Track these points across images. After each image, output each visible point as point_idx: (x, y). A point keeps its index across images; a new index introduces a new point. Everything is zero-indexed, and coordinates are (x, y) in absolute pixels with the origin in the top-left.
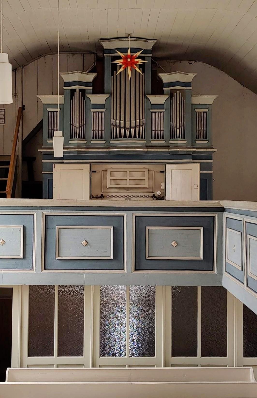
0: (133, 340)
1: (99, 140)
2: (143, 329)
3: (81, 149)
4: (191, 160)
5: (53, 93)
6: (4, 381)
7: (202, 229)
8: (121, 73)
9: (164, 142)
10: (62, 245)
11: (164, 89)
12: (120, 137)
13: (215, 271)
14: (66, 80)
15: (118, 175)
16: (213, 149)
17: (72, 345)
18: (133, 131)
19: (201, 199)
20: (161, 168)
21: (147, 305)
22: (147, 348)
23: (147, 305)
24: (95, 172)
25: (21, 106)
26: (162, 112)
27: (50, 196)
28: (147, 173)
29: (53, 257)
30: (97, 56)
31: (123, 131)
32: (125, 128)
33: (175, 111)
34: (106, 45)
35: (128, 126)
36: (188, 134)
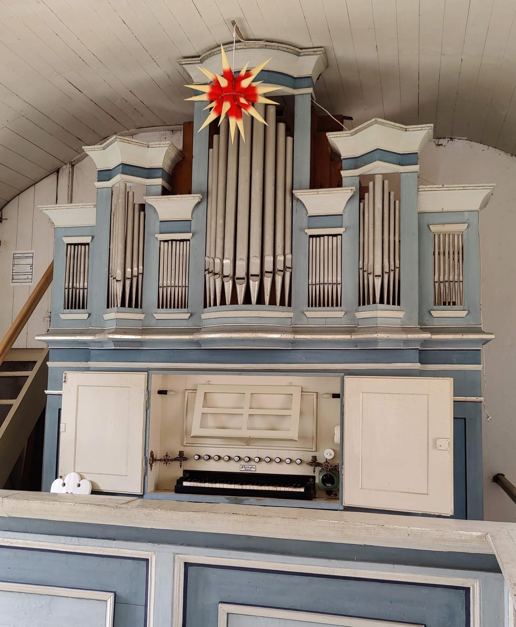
1: (176, 310)
3: (125, 333)
4: (417, 366)
9: (341, 314)
16: (483, 333)
18: (254, 286)
26: (336, 235)
33: (371, 230)
35: (241, 272)
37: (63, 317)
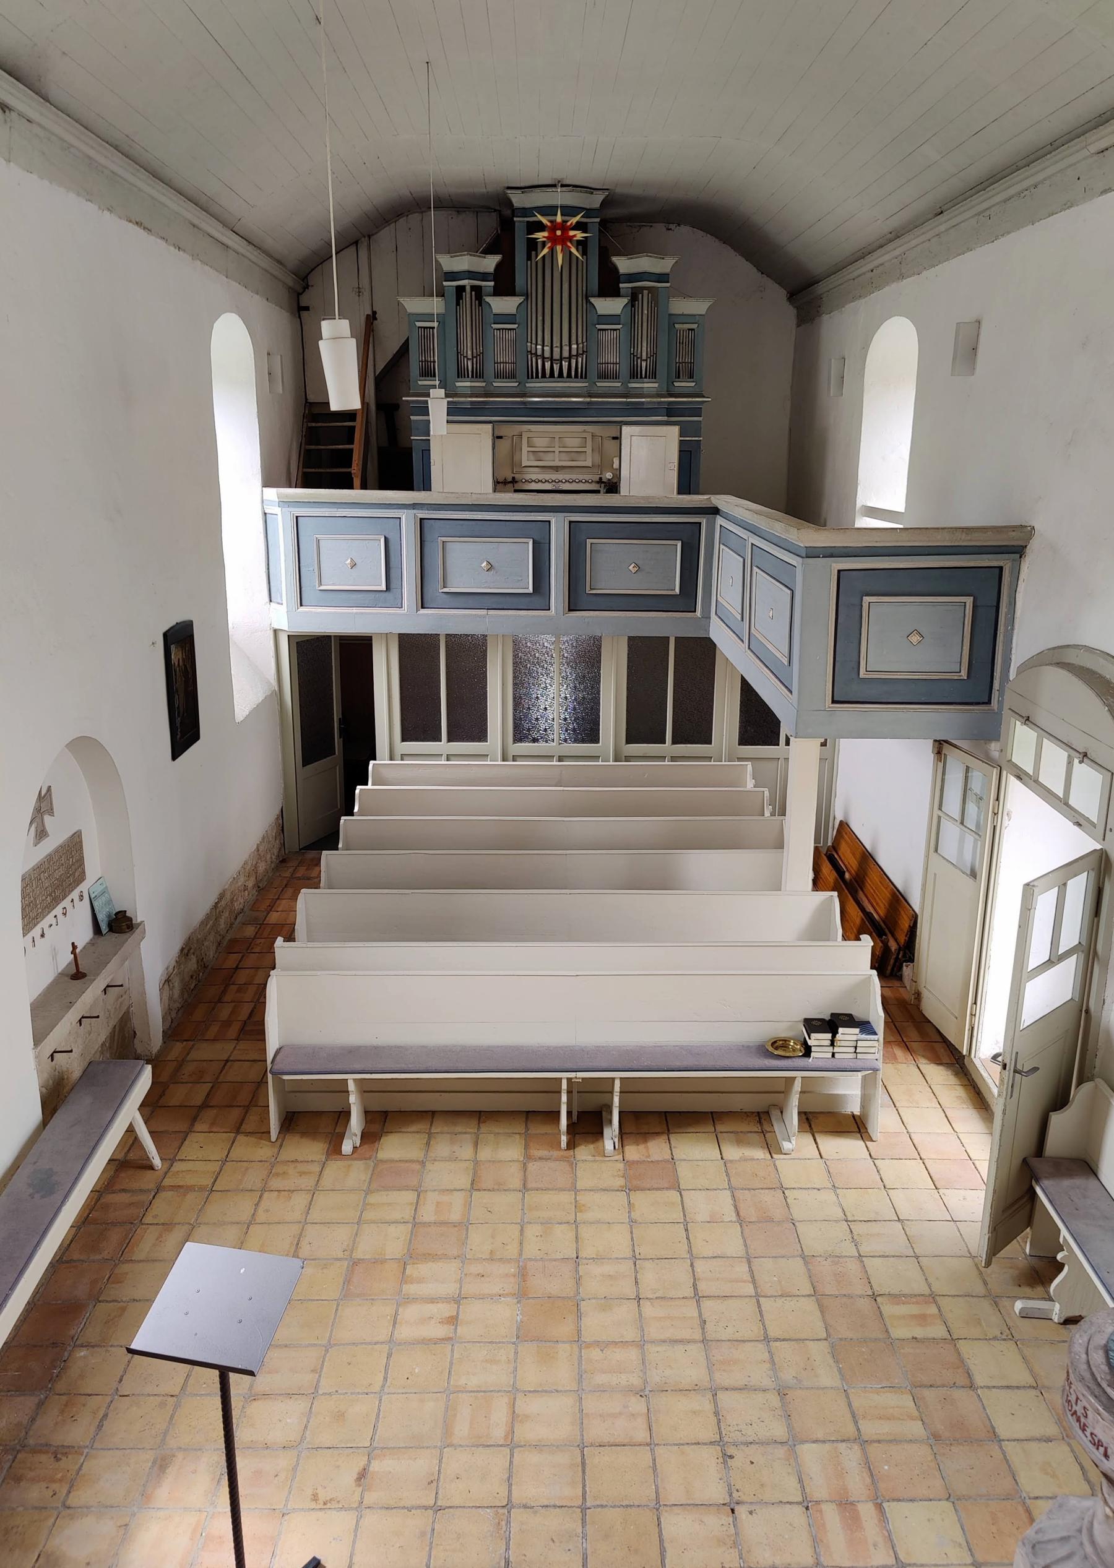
0: (565, 719)
2: (580, 702)
4: (665, 418)
5: (427, 293)
6: (367, 784)
8: (544, 257)
11: (621, 285)
12: (544, 376)
13: (698, 613)
14: (446, 268)
15: (541, 443)
17: (470, 725)
18: (565, 364)
19: (679, 493)
20: (612, 431)
21: (588, 661)
22: (586, 728)
23: (588, 661)
24: (501, 437)
25: (370, 313)
27: (427, 486)
29: (436, 589)
30: (500, 215)
31: (548, 365)
32: (552, 359)
34: (518, 200)
35: (556, 356)
36: (662, 371)
37: (420, 383)
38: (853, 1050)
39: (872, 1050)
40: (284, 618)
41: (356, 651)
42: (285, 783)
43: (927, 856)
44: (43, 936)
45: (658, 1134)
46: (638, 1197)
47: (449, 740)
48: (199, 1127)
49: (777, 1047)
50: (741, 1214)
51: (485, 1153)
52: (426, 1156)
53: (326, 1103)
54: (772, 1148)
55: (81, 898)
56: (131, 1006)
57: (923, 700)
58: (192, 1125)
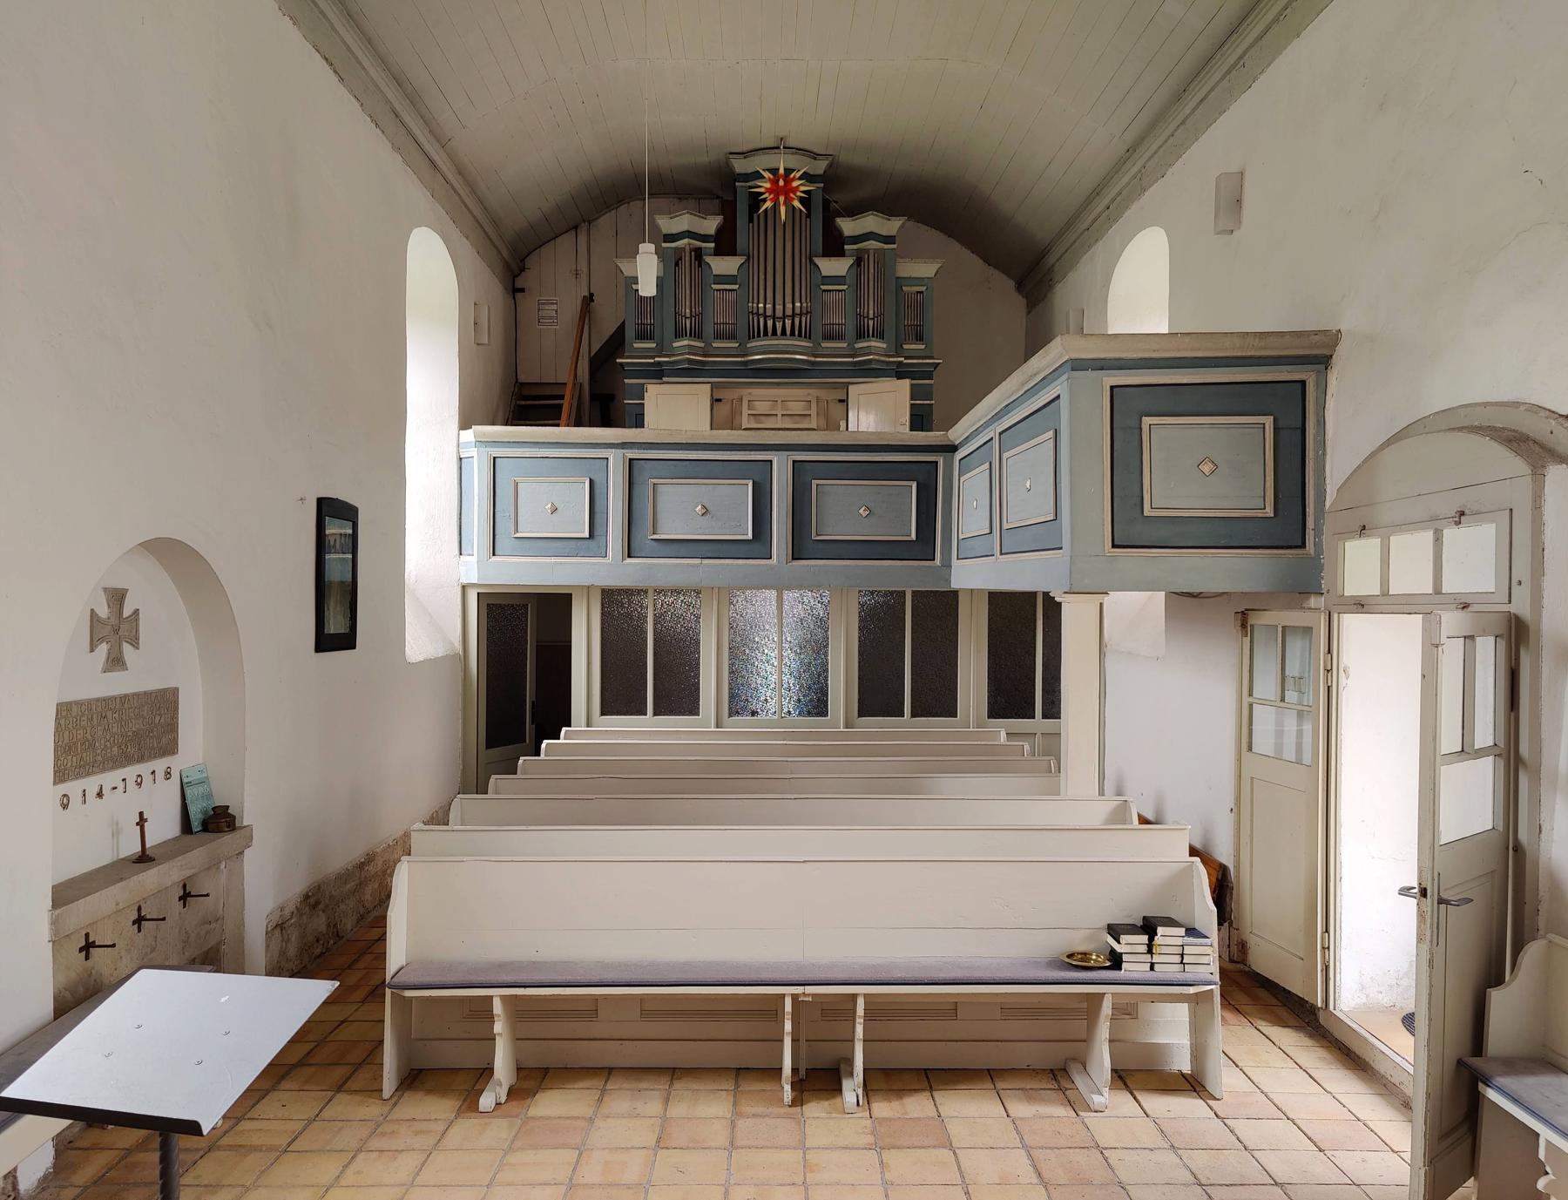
7: (914, 485)
10: (660, 515)
13: (938, 561)
14: (665, 231)
15: (762, 407)
18: (788, 322)
22: (817, 704)
27: (639, 422)
28: (814, 405)
29: (645, 536)
31: (770, 323)
32: (774, 317)
34: (740, 166)
35: (779, 313)
36: (890, 332)
38: (1177, 959)
39: (1205, 960)
40: (475, 569)
41: (553, 608)
42: (464, 761)
43: (1239, 760)
44: (100, 795)
45: (916, 1091)
46: (890, 1156)
47: (655, 714)
48: (285, 1085)
49: (1077, 961)
50: (1044, 1174)
51: (678, 1109)
52: (595, 1113)
53: (465, 1056)
54: (1077, 1104)
55: (168, 775)
56: (219, 943)
57: (1223, 543)
58: (278, 1082)
